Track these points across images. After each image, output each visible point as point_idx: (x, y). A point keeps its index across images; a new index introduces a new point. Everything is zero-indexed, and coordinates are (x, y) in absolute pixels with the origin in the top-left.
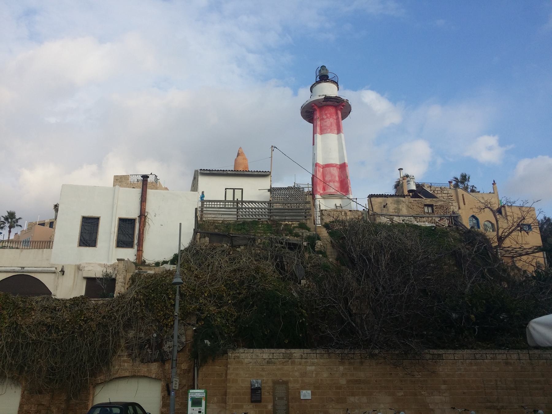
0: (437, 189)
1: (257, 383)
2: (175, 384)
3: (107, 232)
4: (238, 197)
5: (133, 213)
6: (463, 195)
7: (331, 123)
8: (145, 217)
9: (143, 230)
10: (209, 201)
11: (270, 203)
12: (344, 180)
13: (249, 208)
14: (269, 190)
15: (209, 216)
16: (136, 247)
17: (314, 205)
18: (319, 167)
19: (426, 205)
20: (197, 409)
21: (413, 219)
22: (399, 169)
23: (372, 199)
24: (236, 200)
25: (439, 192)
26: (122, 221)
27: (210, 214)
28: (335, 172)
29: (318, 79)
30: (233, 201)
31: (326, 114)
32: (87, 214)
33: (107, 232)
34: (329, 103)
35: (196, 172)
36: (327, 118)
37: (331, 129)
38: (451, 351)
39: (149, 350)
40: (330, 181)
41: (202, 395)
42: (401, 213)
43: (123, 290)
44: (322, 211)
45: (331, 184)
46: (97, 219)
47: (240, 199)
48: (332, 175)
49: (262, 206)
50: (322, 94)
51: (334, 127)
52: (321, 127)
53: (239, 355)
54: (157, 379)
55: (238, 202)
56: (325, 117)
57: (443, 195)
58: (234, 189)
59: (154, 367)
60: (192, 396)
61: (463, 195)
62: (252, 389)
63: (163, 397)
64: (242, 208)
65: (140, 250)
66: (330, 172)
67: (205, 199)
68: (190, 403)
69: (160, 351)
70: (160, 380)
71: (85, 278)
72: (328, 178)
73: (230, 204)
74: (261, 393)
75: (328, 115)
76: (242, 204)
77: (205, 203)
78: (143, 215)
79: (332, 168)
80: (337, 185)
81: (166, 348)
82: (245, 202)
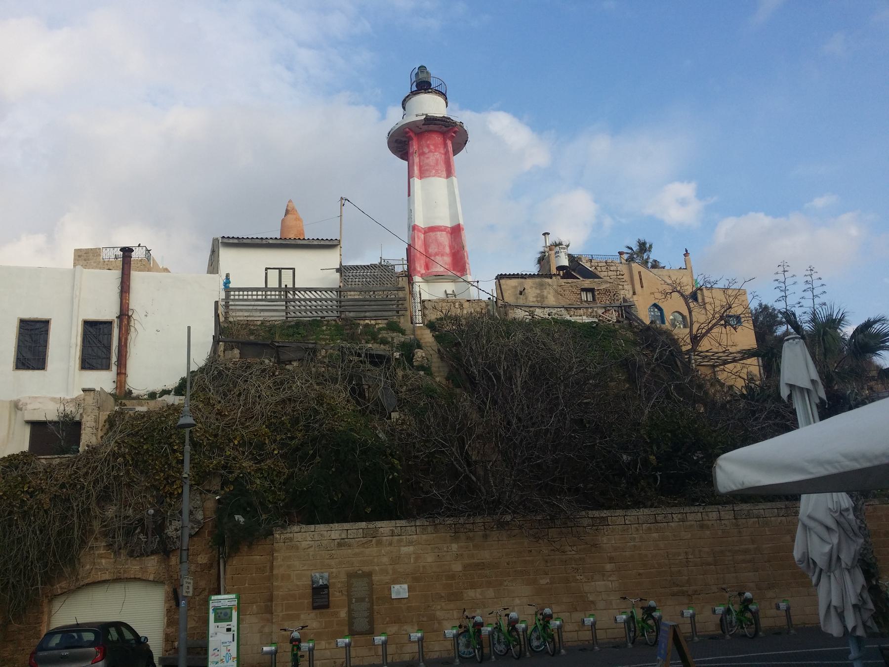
0: (600, 265)
1: (322, 577)
2: (187, 588)
3: (64, 344)
4: (287, 281)
5: (108, 312)
6: (640, 272)
7: (437, 160)
8: (129, 317)
9: (126, 339)
10: (239, 290)
11: (339, 291)
12: (458, 251)
13: (305, 300)
14: (338, 270)
15: (239, 314)
16: (114, 368)
17: (411, 293)
18: (419, 231)
19: (583, 290)
20: (224, 625)
21: (563, 311)
22: (544, 234)
23: (503, 281)
24: (283, 286)
25: (604, 269)
26: (89, 325)
27: (241, 310)
28: (444, 239)
29: (414, 88)
30: (280, 289)
31: (428, 146)
32: (27, 315)
33: (64, 344)
34: (432, 127)
35: (215, 241)
36: (430, 151)
37: (437, 171)
38: (619, 512)
39: (141, 536)
40: (436, 254)
41: (233, 603)
42: (546, 303)
43: (94, 441)
44: (424, 301)
45: (438, 259)
46: (47, 323)
47: (290, 286)
48: (439, 244)
49: (328, 295)
50: (420, 113)
51: (442, 167)
52: (420, 167)
53: (291, 535)
54: (156, 582)
55: (287, 290)
56: (426, 150)
57: (610, 273)
58: (280, 270)
59: (152, 563)
60: (216, 604)
61: (640, 272)
62: (313, 589)
63: (169, 611)
64: (294, 300)
65: (122, 373)
66: (436, 240)
67: (231, 286)
68: (212, 616)
69: (161, 537)
70: (162, 583)
71: (28, 422)
72: (433, 249)
73: (273, 293)
74: (328, 594)
75: (432, 147)
76: (294, 294)
77: (232, 293)
78: (125, 315)
79: (439, 233)
80: (448, 259)
81: (170, 531)
82: (300, 290)
